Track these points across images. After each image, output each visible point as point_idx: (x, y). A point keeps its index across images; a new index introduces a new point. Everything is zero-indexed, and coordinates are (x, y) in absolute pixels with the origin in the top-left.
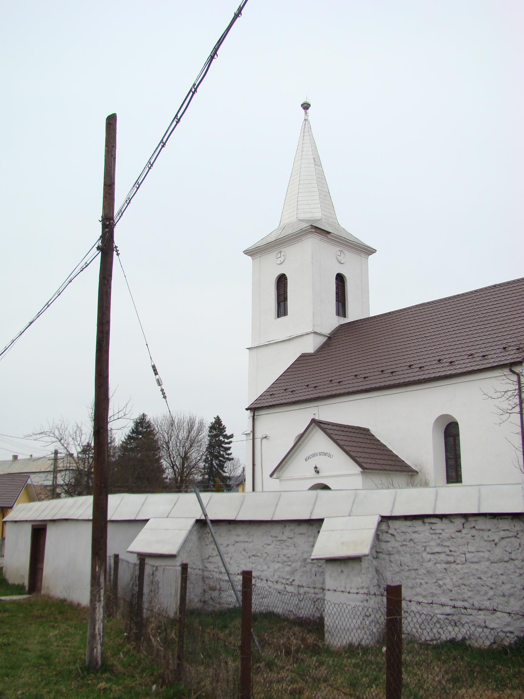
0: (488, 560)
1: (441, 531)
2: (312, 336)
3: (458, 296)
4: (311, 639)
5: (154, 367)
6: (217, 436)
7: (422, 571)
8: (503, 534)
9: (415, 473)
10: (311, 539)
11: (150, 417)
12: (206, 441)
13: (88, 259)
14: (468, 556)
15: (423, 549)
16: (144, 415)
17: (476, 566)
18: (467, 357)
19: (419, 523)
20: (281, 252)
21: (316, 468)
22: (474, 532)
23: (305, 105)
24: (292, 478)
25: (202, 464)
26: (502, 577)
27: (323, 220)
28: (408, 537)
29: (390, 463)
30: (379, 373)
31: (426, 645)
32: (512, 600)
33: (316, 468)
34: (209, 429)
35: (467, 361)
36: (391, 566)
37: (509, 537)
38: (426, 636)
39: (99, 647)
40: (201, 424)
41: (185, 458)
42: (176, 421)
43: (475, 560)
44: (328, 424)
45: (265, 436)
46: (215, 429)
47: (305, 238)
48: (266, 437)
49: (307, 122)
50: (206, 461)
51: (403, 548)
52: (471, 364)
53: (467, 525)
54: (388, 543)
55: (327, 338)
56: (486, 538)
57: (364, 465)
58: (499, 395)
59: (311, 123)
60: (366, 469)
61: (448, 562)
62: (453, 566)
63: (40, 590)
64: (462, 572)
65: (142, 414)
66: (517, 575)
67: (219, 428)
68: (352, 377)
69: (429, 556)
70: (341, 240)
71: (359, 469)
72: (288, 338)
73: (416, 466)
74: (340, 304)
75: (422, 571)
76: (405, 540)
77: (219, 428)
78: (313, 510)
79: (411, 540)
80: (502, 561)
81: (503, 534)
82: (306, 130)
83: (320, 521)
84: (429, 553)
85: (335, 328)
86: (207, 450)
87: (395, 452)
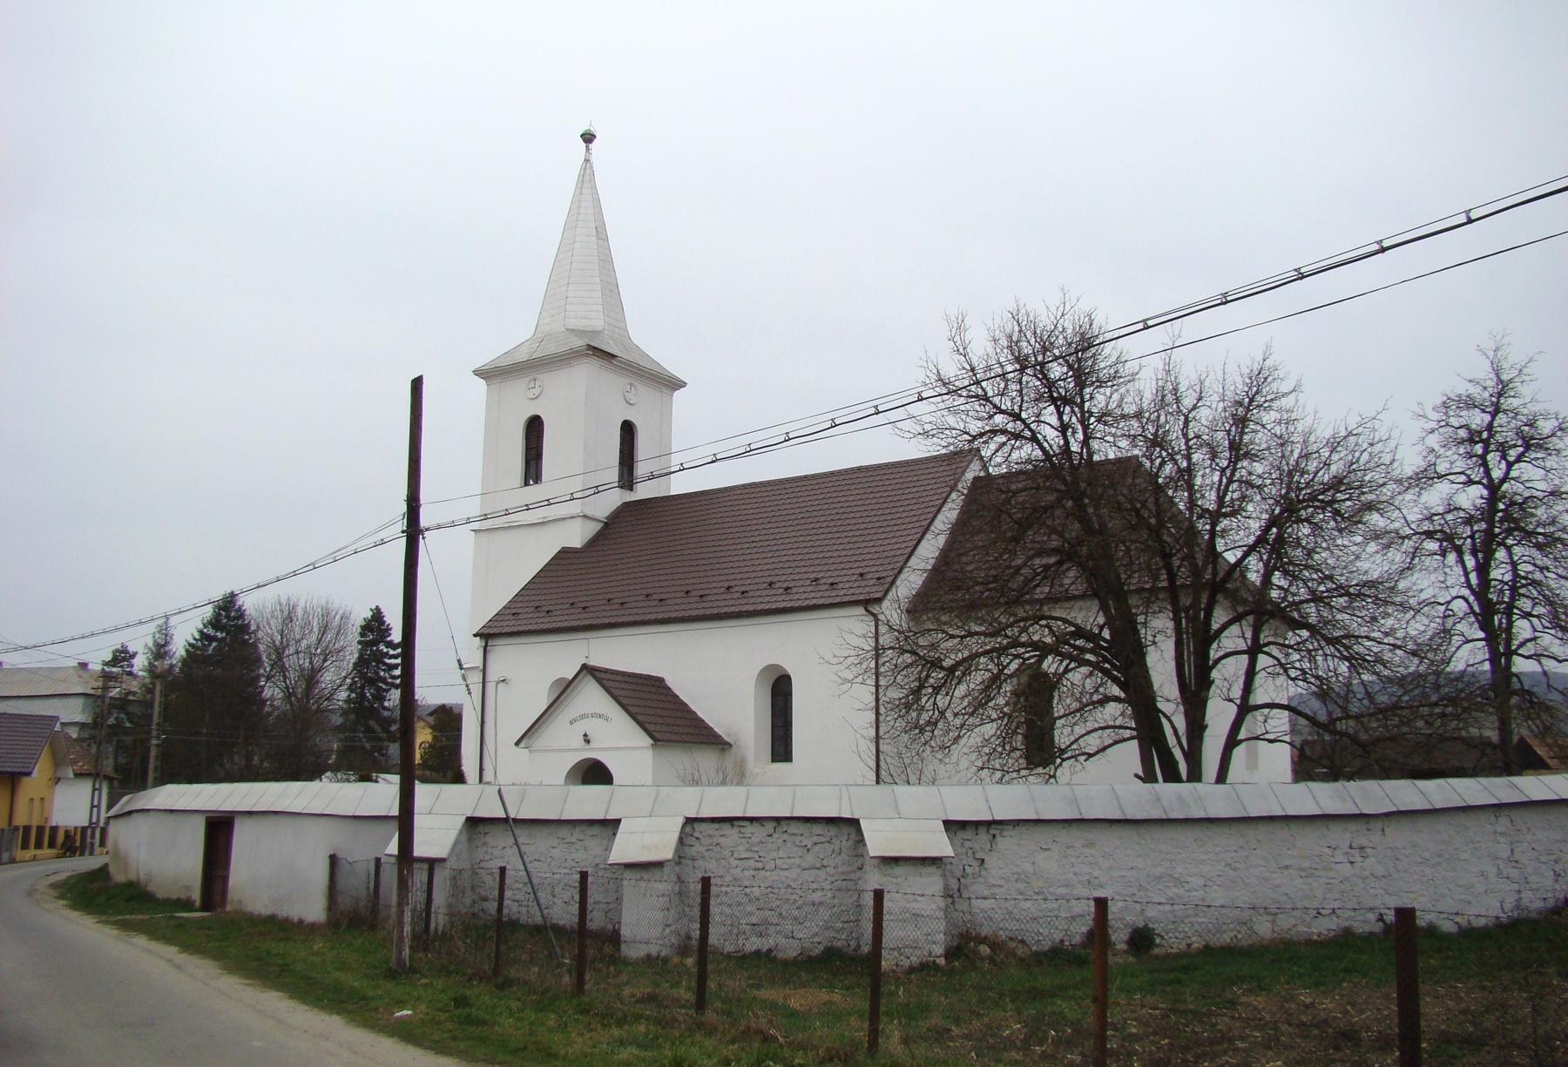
0: (799, 866)
3: (806, 477)
4: (608, 949)
5: (459, 661)
6: (375, 643)
8: (816, 839)
10: (605, 842)
12: (352, 655)
13: (384, 535)
14: (778, 862)
18: (809, 582)
19: (727, 825)
21: (585, 735)
22: (785, 836)
25: (343, 695)
27: (606, 332)
28: (715, 840)
29: (691, 730)
30: (642, 598)
31: (729, 956)
32: (821, 909)
33: (585, 735)
34: (359, 630)
35: (810, 589)
38: (729, 948)
39: (407, 950)
40: (345, 617)
41: (311, 677)
46: (371, 631)
50: (351, 689)
51: (709, 852)
52: (813, 595)
53: (779, 829)
56: (798, 843)
57: (657, 735)
58: (835, 661)
60: (659, 740)
61: (757, 869)
62: (762, 873)
63: (223, 902)
67: (379, 628)
69: (736, 862)
70: (632, 367)
71: (651, 742)
73: (729, 736)
74: (626, 469)
77: (379, 628)
78: (608, 808)
81: (816, 839)
82: (587, 178)
83: (617, 822)
86: (354, 668)
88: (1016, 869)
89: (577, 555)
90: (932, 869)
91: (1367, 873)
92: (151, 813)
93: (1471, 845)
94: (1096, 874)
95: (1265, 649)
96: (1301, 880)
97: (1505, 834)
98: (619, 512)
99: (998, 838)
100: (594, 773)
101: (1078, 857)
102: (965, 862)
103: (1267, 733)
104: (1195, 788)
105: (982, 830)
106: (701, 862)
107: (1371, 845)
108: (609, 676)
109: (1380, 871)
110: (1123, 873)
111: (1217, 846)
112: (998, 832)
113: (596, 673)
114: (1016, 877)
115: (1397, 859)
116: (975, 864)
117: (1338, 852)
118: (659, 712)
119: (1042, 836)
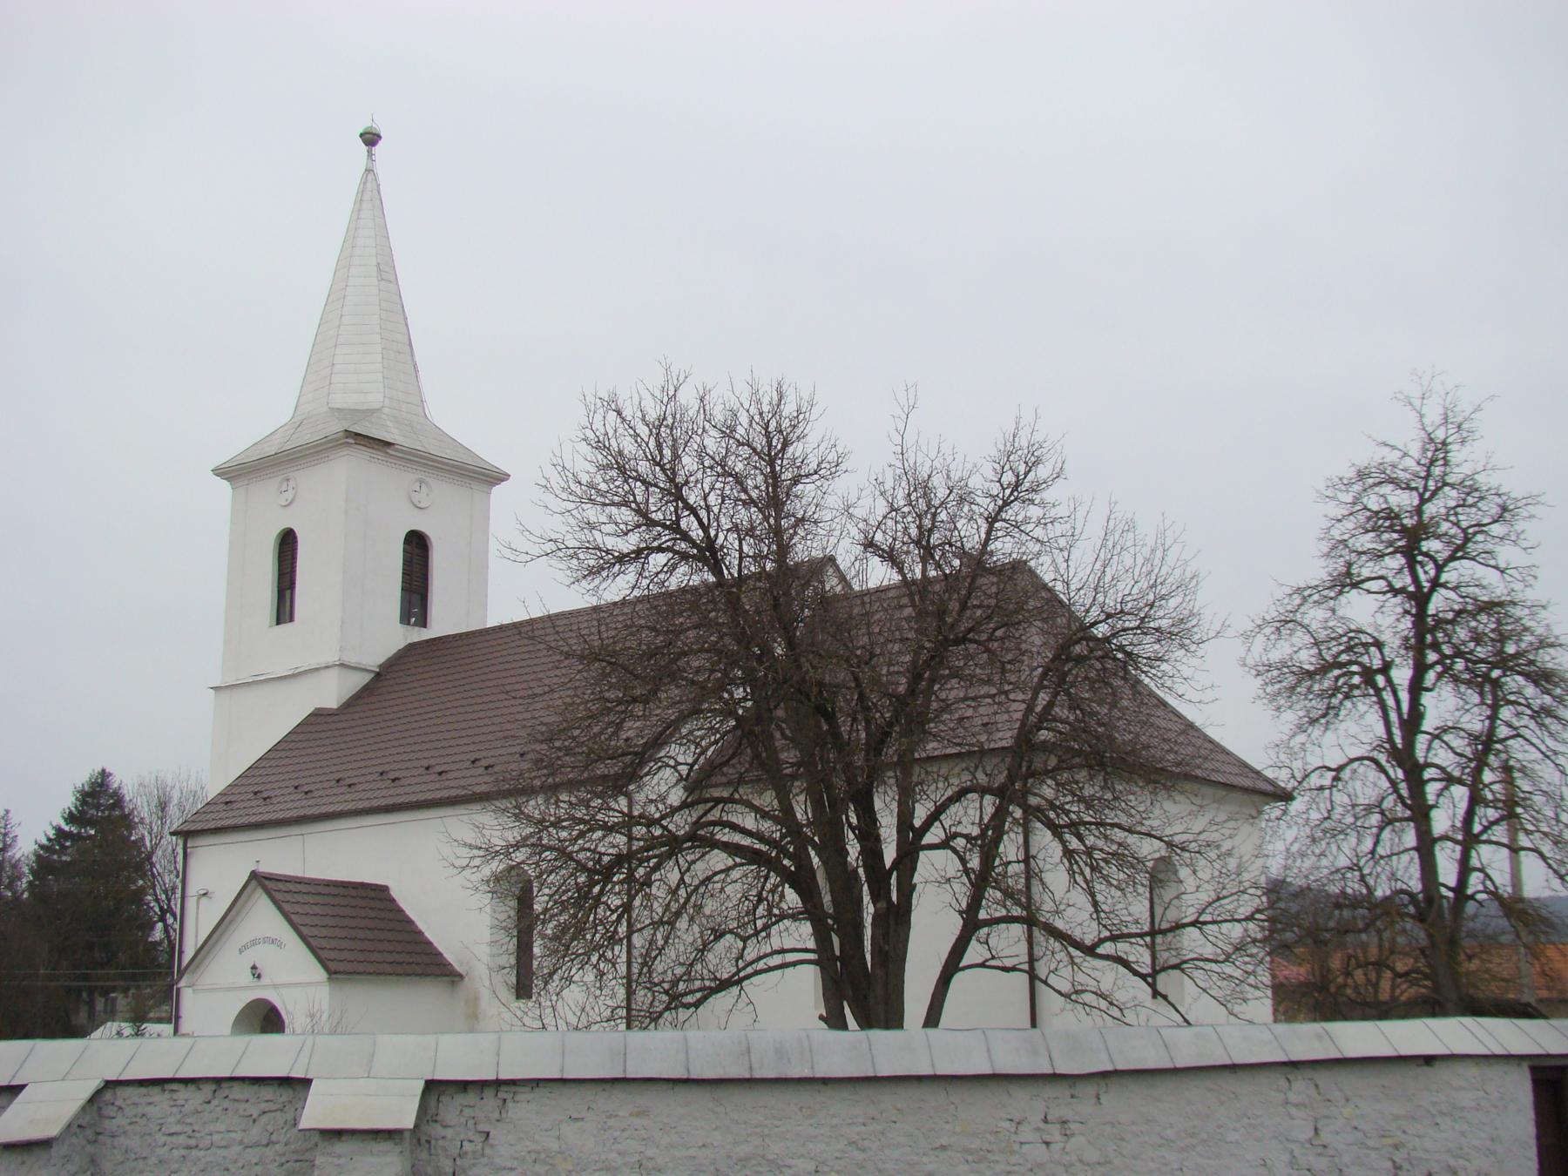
0: (241, 1142)
1: (183, 1103)
2: (335, 672)
8: (264, 1106)
9: (456, 979)
11: (128, 779)
14: (216, 1137)
15: (158, 1128)
16: (104, 774)
17: (224, 1152)
19: (156, 1090)
20: (288, 480)
21: (254, 968)
22: (226, 1104)
23: (368, 136)
24: (215, 987)
26: (257, 1167)
27: (386, 410)
28: (140, 1110)
30: (422, 771)
33: (254, 968)
36: (113, 1154)
37: (270, 1111)
42: (176, 795)
43: (224, 1143)
45: (204, 892)
47: (341, 454)
49: (371, 176)
51: (132, 1127)
53: (221, 1093)
59: (381, 181)
60: (335, 973)
61: (189, 1148)
62: (194, 1152)
64: (204, 1160)
65: (100, 770)
68: (375, 776)
69: (165, 1138)
75: (152, 1160)
79: (143, 1115)
82: (367, 195)
84: (164, 1135)
87: (429, 935)
88: (533, 1146)
91: (1074, 1158)
92: (1440, 1072)
93: (1246, 1121)
94: (650, 1153)
95: (1484, 837)
96: (966, 1167)
97: (1305, 1106)
98: (400, 657)
99: (510, 1104)
100: (266, 1018)
101: (623, 1130)
102: (462, 1136)
103: (993, 958)
106: (122, 1139)
107: (1077, 1118)
108: (281, 886)
109: (1092, 1155)
110: (691, 1152)
111: (834, 1116)
112: (508, 1096)
113: (267, 883)
114: (534, 1156)
115: (1122, 1139)
116: (478, 1139)
117: (1024, 1128)
119: (572, 1101)
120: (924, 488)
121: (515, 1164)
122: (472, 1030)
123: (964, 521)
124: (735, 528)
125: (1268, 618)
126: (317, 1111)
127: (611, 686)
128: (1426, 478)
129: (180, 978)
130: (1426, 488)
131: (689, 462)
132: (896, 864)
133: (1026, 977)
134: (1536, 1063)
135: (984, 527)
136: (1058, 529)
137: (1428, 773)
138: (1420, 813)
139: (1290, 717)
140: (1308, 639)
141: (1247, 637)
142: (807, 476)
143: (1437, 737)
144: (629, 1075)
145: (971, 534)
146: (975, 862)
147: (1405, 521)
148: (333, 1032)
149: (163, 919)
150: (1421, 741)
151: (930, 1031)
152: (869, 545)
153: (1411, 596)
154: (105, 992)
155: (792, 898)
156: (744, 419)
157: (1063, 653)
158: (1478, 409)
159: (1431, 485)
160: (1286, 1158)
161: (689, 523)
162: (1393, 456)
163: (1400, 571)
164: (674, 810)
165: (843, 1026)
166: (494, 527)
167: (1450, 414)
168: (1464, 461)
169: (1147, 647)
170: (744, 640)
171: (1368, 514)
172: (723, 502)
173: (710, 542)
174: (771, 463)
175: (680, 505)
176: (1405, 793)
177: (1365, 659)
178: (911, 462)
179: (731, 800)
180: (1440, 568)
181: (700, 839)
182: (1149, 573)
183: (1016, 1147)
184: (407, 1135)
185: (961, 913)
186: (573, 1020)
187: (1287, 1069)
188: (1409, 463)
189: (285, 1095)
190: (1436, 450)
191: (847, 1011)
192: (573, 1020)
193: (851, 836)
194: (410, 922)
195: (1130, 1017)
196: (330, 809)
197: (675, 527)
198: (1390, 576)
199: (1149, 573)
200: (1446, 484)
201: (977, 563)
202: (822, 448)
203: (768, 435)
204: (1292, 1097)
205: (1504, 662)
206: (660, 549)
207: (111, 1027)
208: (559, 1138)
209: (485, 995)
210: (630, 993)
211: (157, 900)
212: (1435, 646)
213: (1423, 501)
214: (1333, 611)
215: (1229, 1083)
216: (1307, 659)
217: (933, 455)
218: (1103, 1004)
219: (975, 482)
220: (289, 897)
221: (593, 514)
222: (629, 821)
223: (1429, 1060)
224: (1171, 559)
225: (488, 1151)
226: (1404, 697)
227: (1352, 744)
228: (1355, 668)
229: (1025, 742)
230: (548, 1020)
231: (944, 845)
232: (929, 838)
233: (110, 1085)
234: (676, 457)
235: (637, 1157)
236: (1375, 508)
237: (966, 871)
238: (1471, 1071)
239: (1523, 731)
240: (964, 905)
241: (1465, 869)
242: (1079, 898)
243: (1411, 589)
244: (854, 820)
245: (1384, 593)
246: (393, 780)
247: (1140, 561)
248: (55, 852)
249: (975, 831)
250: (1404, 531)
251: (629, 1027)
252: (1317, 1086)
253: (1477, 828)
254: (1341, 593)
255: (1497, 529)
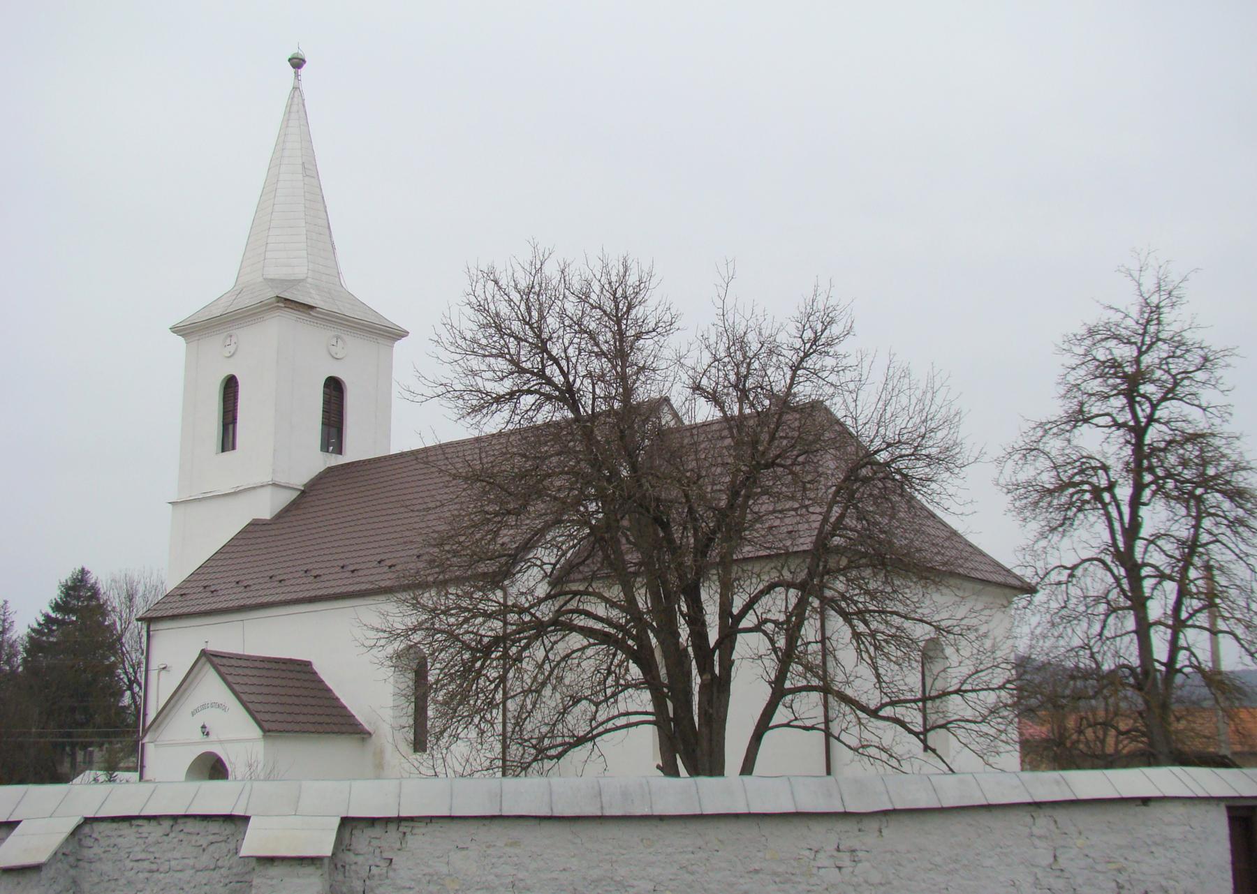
0: (193, 867)
1: (147, 835)
2: (269, 489)
7: (122, 881)
8: (211, 838)
11: (103, 576)
14: (173, 863)
15: (127, 855)
17: (179, 875)
19: (125, 825)
20: (231, 336)
21: (204, 727)
22: (182, 836)
23: (295, 60)
26: (206, 887)
27: (309, 280)
28: (112, 841)
30: (338, 569)
42: (141, 589)
44: (229, 658)
48: (164, 668)
49: (297, 93)
51: (106, 855)
54: (92, 850)
55: (299, 493)
59: (305, 96)
60: (269, 731)
61: (151, 871)
62: (156, 875)
66: (222, 884)
69: (132, 864)
72: (233, 491)
75: (122, 881)
76: (108, 846)
79: (115, 845)
80: (207, 870)
82: (295, 108)
84: (132, 861)
85: (317, 473)
89: (264, 528)
90: (310, 870)
92: (1155, 811)
93: (999, 850)
94: (520, 876)
95: (1190, 622)
96: (775, 887)
97: (1046, 837)
99: (408, 836)
100: (213, 768)
101: (500, 857)
102: (371, 862)
103: (796, 719)
104: (742, 781)
105: (392, 827)
106: (98, 865)
107: (863, 848)
108: (225, 661)
109: (875, 877)
110: (554, 875)
112: (407, 830)
114: (428, 878)
115: (900, 865)
116: (384, 864)
118: (284, 699)
120: (741, 342)
121: (413, 884)
122: (378, 777)
123: (772, 369)
124: (590, 375)
125: (1016, 446)
126: (255, 842)
127: (490, 501)
128: (1143, 335)
129: (144, 736)
130: (1143, 343)
131: (552, 322)
132: (718, 644)
133: (822, 734)
134: (1231, 803)
135: (789, 374)
136: (849, 375)
137: (1145, 571)
138: (1139, 603)
139: (1034, 526)
140: (1048, 464)
141: (1000, 461)
142: (647, 333)
143: (1152, 542)
144: (504, 813)
145: (778, 379)
146: (781, 643)
147: (1127, 369)
148: (267, 779)
149: (130, 688)
150: (1139, 546)
151: (746, 778)
152: (697, 388)
153: (1131, 429)
154: (84, 746)
155: (635, 671)
156: (596, 287)
157: (852, 475)
158: (1185, 279)
159: (1147, 340)
160: (1031, 879)
161: (552, 371)
162: (1117, 317)
163: (1123, 409)
164: (541, 601)
165: (676, 774)
166: (396, 374)
167: (1162, 283)
168: (1173, 321)
169: (920, 470)
170: (596, 464)
171: (1097, 363)
172: (579, 354)
173: (569, 386)
174: (618, 323)
175: (545, 356)
176: (1126, 587)
177: (1094, 480)
178: (731, 321)
179: (586, 593)
180: (1154, 407)
181: (561, 624)
182: (922, 411)
183: (815, 871)
184: (326, 861)
185: (770, 683)
186: (459, 769)
187: (1031, 808)
188: (1130, 323)
189: (228, 829)
190: (1152, 312)
191: (679, 762)
192: (459, 769)
193: (682, 621)
194: (329, 690)
195: (906, 767)
196: (265, 600)
197: (541, 374)
198: (1114, 412)
199: (922, 411)
200: (1159, 340)
201: (784, 403)
202: (659, 311)
203: (615, 300)
204: (1036, 831)
205: (1206, 482)
206: (529, 392)
207: (89, 775)
208: (448, 863)
209: (389, 749)
210: (505, 748)
211: (126, 673)
212: (1151, 469)
213: (1141, 353)
214: (1069, 441)
215: (985, 819)
216: (1048, 480)
217: (748, 316)
218: (884, 756)
219: (782, 338)
220: (231, 670)
221: (475, 363)
222: (505, 610)
223: (1145, 801)
224: (938, 400)
225: (391, 874)
226: (1126, 510)
227: (1084, 548)
228: (1086, 487)
229: (822, 547)
230: (440, 769)
231: (757, 628)
232: (744, 624)
233: (88, 821)
234: (542, 318)
235: (511, 879)
236: (1102, 358)
237: (775, 650)
238: (1179, 810)
239: (1221, 537)
240: (773, 677)
241: (1174, 648)
242: (865, 671)
243: (1132, 423)
244: (684, 609)
245: (1110, 427)
246: (315, 577)
247: (914, 401)
248: (43, 634)
249: (782, 618)
250: (1125, 377)
251: (504, 774)
252: (1056, 822)
253: (1184, 615)
254: (1075, 426)
255: (1200, 376)
